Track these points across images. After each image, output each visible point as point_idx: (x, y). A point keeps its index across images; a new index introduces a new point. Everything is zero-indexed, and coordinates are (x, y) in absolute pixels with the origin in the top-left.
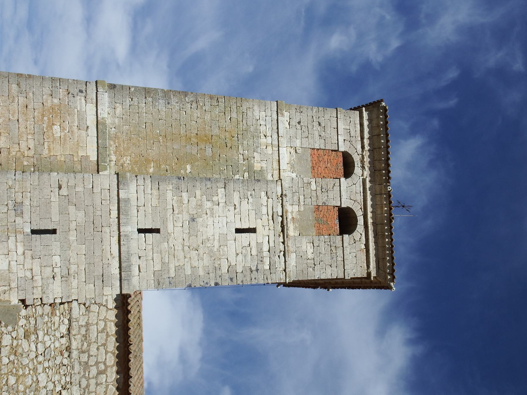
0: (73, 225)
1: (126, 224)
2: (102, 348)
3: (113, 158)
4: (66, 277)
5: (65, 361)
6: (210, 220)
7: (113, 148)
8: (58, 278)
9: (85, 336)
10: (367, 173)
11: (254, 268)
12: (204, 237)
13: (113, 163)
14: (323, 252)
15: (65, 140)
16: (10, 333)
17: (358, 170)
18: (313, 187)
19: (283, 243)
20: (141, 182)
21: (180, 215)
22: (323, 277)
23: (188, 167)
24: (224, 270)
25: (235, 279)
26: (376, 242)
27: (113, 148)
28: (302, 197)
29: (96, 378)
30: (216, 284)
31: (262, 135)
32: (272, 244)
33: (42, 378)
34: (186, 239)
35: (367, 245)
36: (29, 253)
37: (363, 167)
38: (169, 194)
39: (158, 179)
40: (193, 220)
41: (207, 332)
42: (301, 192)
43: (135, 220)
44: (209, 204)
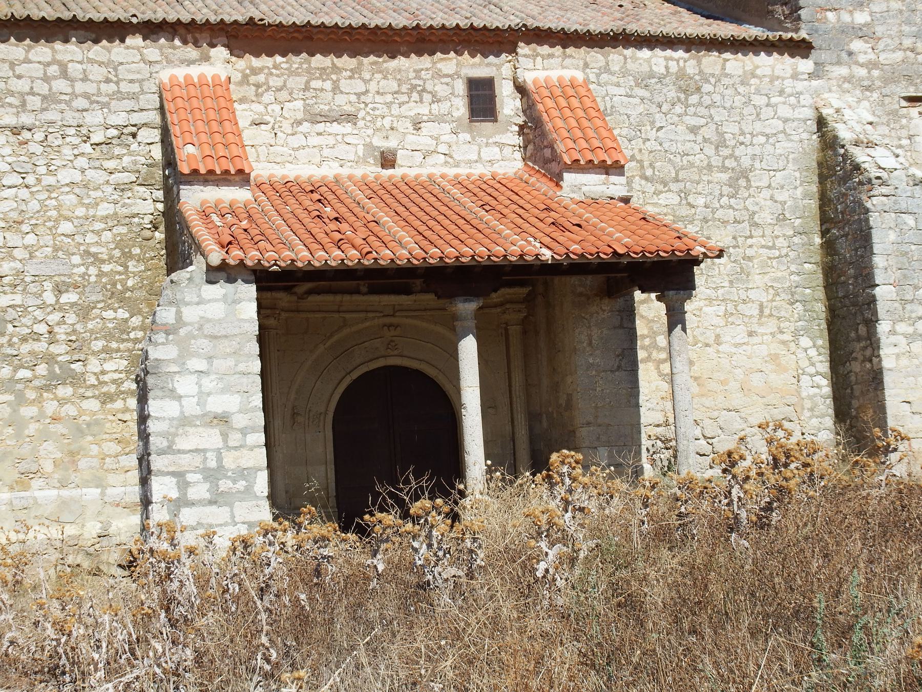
2: (19, 70)
5: (39, 136)
29: (73, 81)
33: (65, 176)
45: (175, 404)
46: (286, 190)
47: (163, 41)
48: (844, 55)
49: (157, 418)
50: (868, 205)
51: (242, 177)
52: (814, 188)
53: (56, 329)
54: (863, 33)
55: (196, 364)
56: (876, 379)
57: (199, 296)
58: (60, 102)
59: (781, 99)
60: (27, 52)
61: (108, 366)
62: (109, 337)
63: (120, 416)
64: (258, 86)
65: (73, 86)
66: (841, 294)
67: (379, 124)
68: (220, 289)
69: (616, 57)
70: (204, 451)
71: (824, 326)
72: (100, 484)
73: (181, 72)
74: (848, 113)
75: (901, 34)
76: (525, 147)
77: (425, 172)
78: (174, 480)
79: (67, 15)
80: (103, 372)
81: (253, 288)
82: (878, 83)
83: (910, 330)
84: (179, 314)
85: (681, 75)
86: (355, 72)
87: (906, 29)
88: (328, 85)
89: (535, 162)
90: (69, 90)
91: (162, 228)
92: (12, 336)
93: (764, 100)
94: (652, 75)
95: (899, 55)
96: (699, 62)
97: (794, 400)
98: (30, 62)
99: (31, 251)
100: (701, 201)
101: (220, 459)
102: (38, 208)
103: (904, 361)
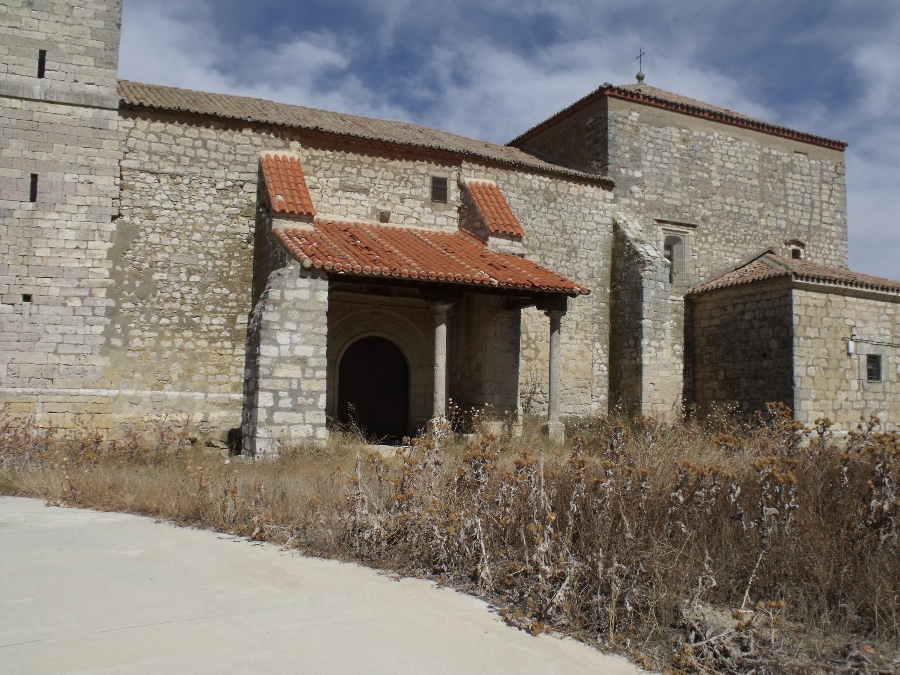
0: (28, 154)
1: (31, 91)
2: (178, 141)
4: (91, 169)
5: (187, 181)
8: (91, 178)
9: (162, 157)
16: (147, 235)
21: (24, 20)
29: (209, 151)
33: (200, 206)
36: (59, 207)
43: (26, 80)
45: (276, 349)
46: (330, 228)
47: (264, 134)
48: (628, 193)
49: (265, 357)
50: (643, 275)
51: (309, 218)
52: (609, 262)
53: (186, 297)
54: (639, 182)
55: (291, 326)
56: (638, 370)
57: (295, 285)
58: (201, 162)
59: (596, 212)
60: (185, 131)
61: (215, 321)
62: (217, 304)
63: (219, 352)
64: (315, 167)
65: (209, 154)
66: (620, 322)
67: (381, 197)
68: (305, 283)
69: (514, 176)
70: (291, 379)
71: (608, 338)
72: (204, 390)
73: (273, 154)
74: (629, 223)
75: (657, 186)
76: (461, 220)
78: (272, 395)
80: (212, 325)
81: (327, 283)
82: (643, 210)
83: (658, 345)
84: (282, 295)
85: (547, 191)
86: (371, 165)
87: (659, 184)
88: (355, 171)
89: (467, 229)
90: (207, 156)
91: (253, 243)
92: (160, 298)
93: (587, 211)
94: (532, 189)
95: (655, 197)
96: (557, 186)
97: (590, 377)
98: (186, 137)
99: (175, 248)
100: (552, 262)
101: (299, 384)
102: (182, 223)
103: (653, 362)
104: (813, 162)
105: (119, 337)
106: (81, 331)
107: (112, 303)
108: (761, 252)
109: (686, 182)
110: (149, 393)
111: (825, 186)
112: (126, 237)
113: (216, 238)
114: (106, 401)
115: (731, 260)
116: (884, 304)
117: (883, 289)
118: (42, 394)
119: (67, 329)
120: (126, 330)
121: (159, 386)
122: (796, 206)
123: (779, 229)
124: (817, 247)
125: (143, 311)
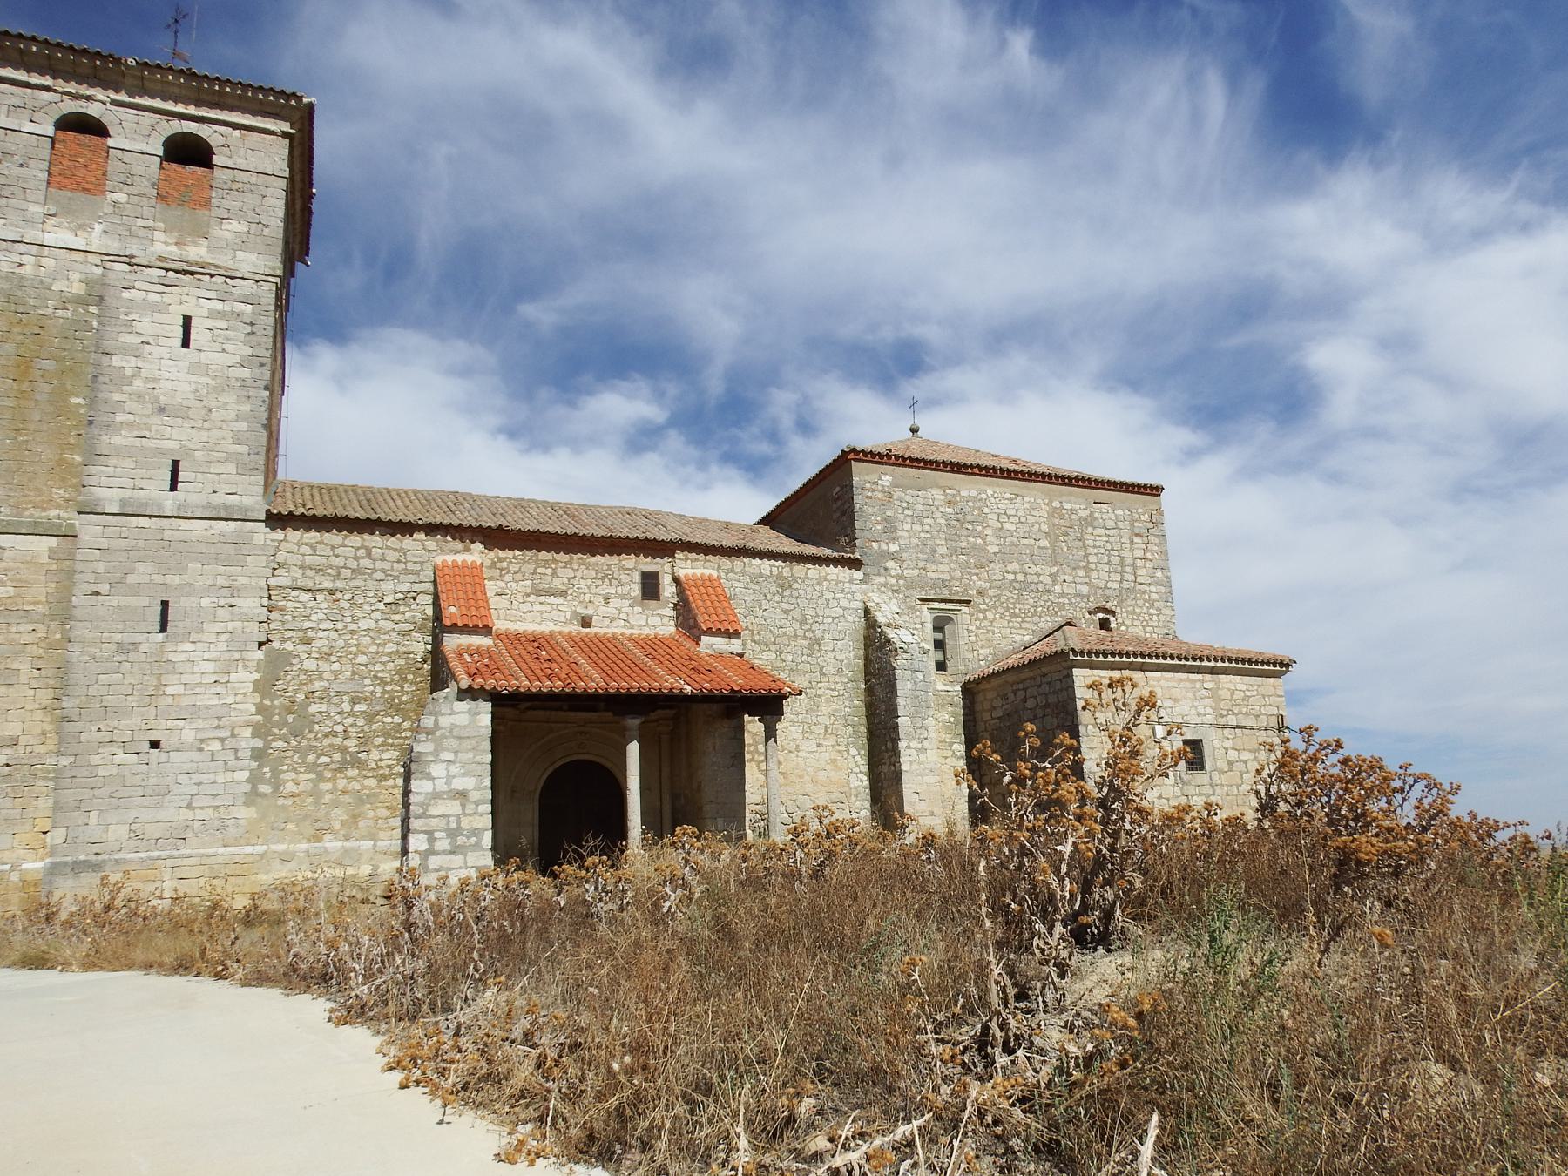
0: (157, 578)
1: (160, 506)
2: (337, 551)
3: (53, 513)
4: (233, 590)
5: (348, 596)
6: (163, 384)
7: (37, 513)
8: (233, 601)
10: (99, 93)
11: (249, 329)
12: (192, 396)
13: (63, 514)
14: (238, 204)
15: (20, 581)
16: (301, 661)
17: (94, 110)
18: (122, 198)
19: (212, 276)
20: (93, 481)
21: (154, 428)
22: (281, 213)
23: (74, 400)
24: (246, 373)
25: (263, 360)
26: (232, 109)
27: (37, 513)
28: (140, 222)
30: (266, 388)
31: (17, 271)
32: (212, 295)
33: (364, 624)
34: (193, 423)
35: (235, 126)
37: (88, 98)
38: (116, 440)
39: (93, 456)
40: (162, 410)
41: (412, 339)
42: (131, 221)
43: (155, 494)
44: (138, 383)
51: (487, 630)
54: (893, 556)
56: (897, 777)
61: (384, 756)
62: (387, 735)
69: (738, 563)
73: (450, 558)
74: (883, 606)
77: (611, 631)
79: (374, 517)
84: (436, 721)
85: (780, 576)
88: (549, 571)
94: (761, 576)
95: (916, 572)
99: (336, 675)
100: (790, 658)
101: (459, 822)
103: (915, 766)
104: (1120, 512)
105: (268, 782)
106: (220, 779)
107: (259, 743)
108: (1057, 626)
109: (954, 551)
110: (304, 846)
111: (1136, 539)
112: (276, 665)
113: (385, 659)
114: (250, 859)
115: (1018, 638)
116: (1200, 676)
117: (1194, 659)
118: (171, 857)
119: (204, 778)
120: (276, 773)
121: (317, 838)
122: (1100, 567)
123: (1078, 595)
124: (1133, 613)
125: (297, 750)
